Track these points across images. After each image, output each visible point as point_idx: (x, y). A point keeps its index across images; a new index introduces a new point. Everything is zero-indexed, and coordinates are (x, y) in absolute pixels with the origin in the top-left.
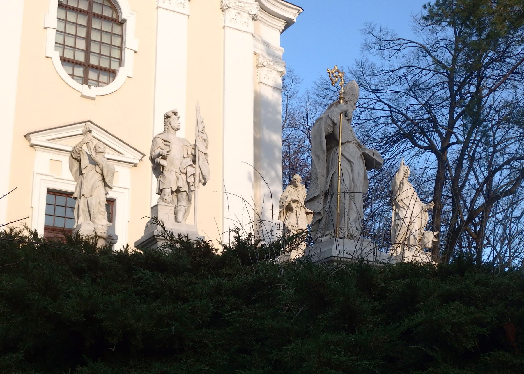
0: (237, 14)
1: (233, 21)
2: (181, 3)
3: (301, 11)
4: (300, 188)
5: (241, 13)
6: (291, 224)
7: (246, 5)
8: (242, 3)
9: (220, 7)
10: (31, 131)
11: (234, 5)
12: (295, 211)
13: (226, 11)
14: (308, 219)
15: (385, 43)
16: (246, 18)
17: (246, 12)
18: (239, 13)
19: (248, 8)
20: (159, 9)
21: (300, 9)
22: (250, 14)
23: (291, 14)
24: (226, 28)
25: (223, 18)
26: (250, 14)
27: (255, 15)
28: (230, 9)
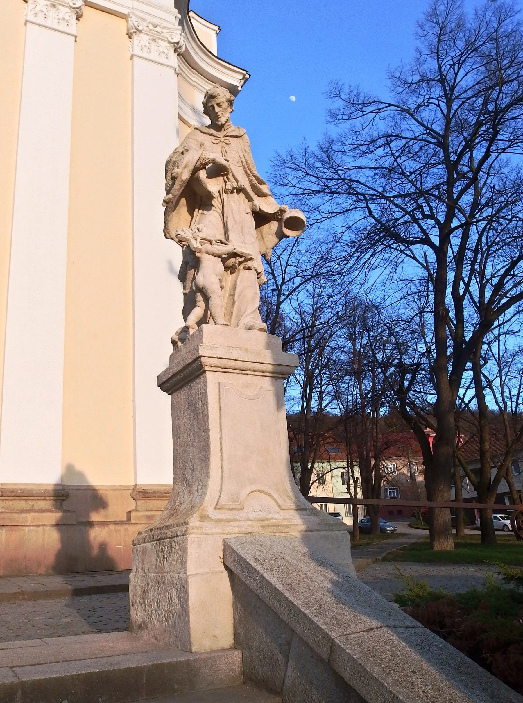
0: (151, 41)
1: (145, 49)
2: (64, 19)
3: (248, 76)
4: (232, 130)
5: (157, 40)
6: (202, 235)
7: (165, 31)
8: (158, 27)
9: (126, 32)
10: (218, 406)
11: (145, 28)
12: (216, 202)
13: (135, 37)
14: (262, 237)
15: (358, 105)
16: (65, 12)
17: (164, 40)
18: (154, 40)
19: (166, 34)
20: (28, 24)
21: (245, 73)
22: (170, 42)
23: (234, 79)
24: (135, 58)
25: (131, 46)
26: (170, 42)
27: (178, 43)
28: (141, 35)
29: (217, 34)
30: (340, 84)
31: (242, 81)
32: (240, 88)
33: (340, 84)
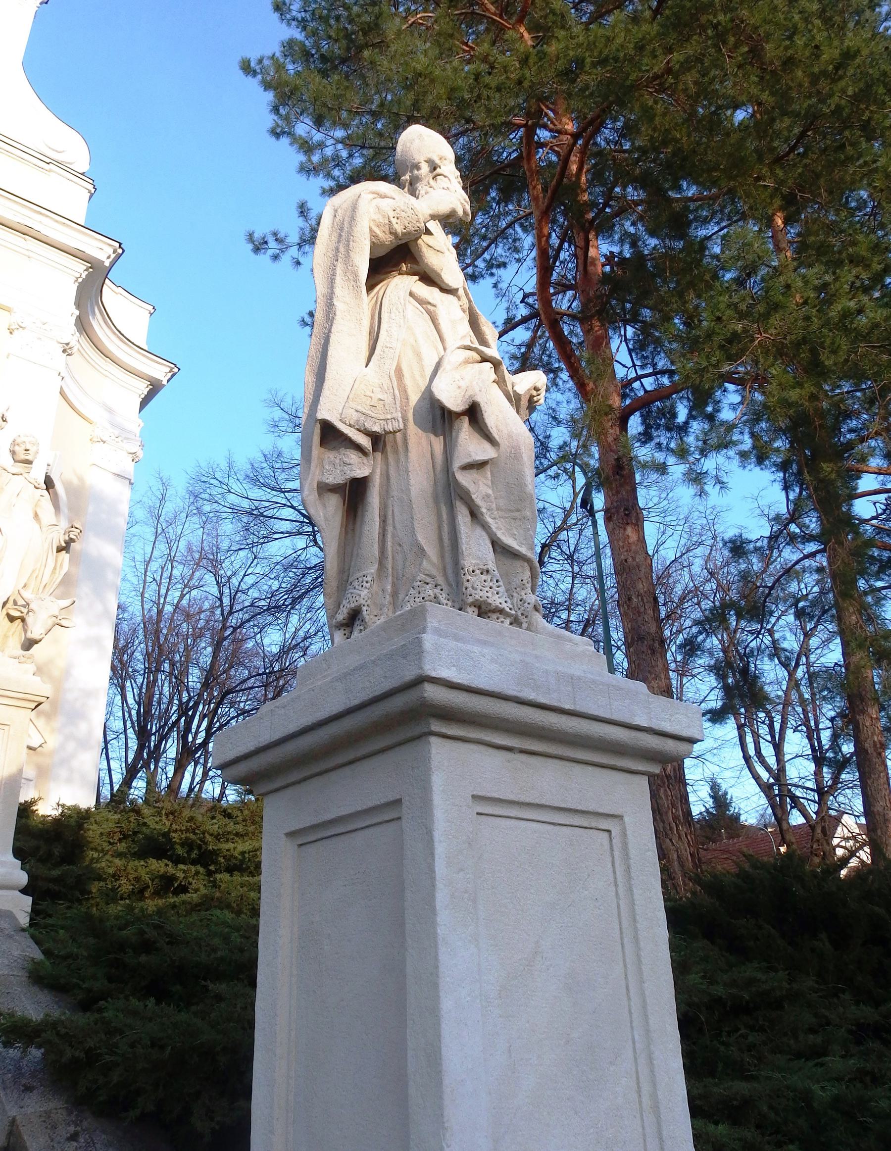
3: (176, 370)
29: (151, 314)
30: (280, 394)
31: (169, 375)
32: (165, 382)
33: (280, 394)
